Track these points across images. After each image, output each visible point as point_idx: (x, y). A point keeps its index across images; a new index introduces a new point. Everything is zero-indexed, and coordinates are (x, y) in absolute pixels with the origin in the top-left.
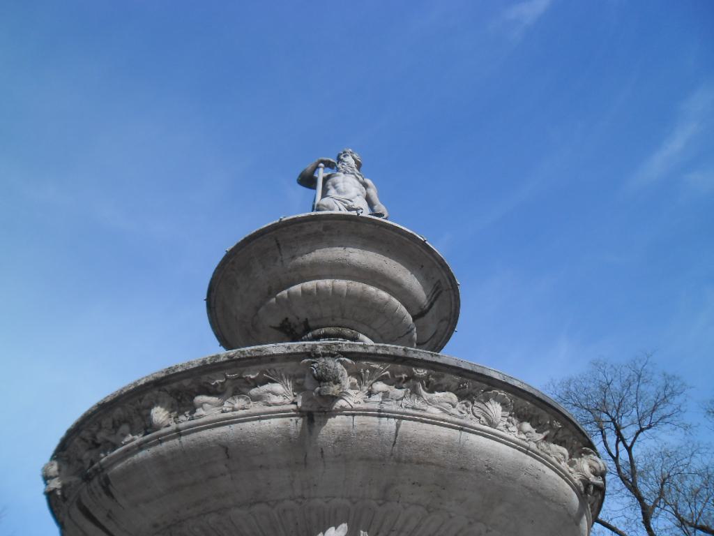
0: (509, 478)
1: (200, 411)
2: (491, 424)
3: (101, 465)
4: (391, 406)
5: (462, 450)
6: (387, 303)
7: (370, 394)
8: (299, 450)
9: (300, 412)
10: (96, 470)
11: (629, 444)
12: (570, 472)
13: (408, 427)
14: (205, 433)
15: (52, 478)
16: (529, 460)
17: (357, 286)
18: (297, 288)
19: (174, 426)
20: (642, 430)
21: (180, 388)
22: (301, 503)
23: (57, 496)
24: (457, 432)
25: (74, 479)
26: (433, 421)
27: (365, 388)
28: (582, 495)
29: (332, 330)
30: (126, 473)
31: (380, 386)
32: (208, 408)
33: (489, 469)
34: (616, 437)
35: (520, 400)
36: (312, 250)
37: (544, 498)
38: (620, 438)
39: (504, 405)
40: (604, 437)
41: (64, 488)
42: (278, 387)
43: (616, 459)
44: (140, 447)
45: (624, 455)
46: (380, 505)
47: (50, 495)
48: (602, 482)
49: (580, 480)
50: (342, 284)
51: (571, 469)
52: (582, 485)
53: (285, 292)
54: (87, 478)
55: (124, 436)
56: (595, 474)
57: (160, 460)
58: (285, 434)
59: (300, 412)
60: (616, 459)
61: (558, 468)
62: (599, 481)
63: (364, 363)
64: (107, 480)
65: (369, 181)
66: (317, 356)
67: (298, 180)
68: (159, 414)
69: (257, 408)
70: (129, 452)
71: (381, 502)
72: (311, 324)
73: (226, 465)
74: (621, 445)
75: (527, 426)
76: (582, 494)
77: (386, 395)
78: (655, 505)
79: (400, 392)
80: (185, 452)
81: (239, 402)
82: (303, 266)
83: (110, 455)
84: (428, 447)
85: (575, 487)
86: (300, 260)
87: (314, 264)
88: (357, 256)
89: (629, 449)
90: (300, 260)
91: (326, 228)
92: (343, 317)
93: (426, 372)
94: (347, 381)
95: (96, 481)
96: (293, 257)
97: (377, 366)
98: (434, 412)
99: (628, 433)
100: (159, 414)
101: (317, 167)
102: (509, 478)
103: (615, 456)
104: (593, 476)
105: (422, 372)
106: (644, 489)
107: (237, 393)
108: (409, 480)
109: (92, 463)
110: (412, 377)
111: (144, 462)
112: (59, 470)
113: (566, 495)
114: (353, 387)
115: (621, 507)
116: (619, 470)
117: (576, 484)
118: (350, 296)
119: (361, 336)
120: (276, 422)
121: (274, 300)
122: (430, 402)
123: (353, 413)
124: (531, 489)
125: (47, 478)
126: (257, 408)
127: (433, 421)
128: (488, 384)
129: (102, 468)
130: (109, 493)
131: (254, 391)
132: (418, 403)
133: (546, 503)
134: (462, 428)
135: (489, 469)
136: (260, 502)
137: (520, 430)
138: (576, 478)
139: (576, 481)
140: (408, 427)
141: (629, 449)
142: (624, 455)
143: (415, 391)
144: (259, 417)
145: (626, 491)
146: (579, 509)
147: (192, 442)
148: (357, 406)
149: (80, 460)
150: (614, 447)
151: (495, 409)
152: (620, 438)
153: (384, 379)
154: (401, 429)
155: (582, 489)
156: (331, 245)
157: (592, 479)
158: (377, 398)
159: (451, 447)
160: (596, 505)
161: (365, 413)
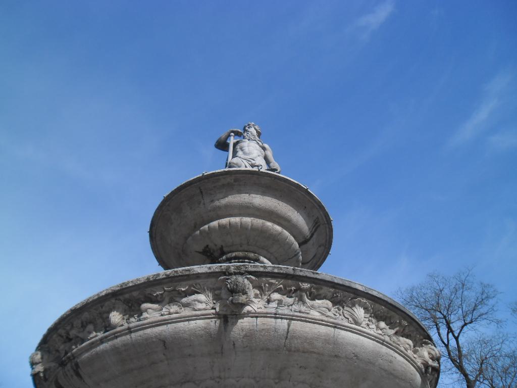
0: (371, 363)
1: (145, 315)
2: (357, 323)
3: (73, 355)
4: (284, 310)
6: (280, 234)
7: (269, 301)
8: (218, 342)
9: (218, 315)
10: (69, 358)
11: (456, 335)
12: (414, 357)
13: (297, 326)
14: (149, 331)
15: (37, 364)
16: (384, 349)
17: (258, 222)
18: (215, 224)
19: (126, 325)
20: (466, 324)
21: (130, 298)
22: (219, 382)
23: (40, 377)
25: (53, 364)
26: (314, 321)
27: (265, 298)
28: (423, 375)
29: (241, 254)
30: (91, 360)
31: (276, 296)
32: (151, 312)
34: (447, 329)
36: (224, 197)
37: (396, 377)
38: (450, 330)
39: (366, 309)
40: (438, 329)
41: (45, 371)
42: (202, 297)
43: (447, 346)
44: (102, 341)
45: (453, 343)
46: (276, 383)
47: (35, 376)
48: (438, 365)
49: (422, 363)
50: (247, 220)
51: (415, 356)
52: (423, 367)
53: (206, 226)
54: (62, 364)
55: (90, 333)
56: (433, 359)
57: (115, 350)
59: (218, 315)
60: (447, 346)
61: (405, 354)
62: (435, 364)
64: (77, 365)
65: (266, 146)
66: (231, 274)
67: (215, 145)
68: (115, 317)
69: (187, 312)
70: (93, 345)
71: (277, 381)
72: (225, 249)
73: (164, 354)
74: (450, 335)
75: (382, 324)
76: (423, 374)
77: (280, 302)
78: (476, 380)
79: (291, 300)
80: (134, 345)
81: (174, 308)
82: (219, 208)
83: (79, 347)
85: (418, 369)
86: (217, 203)
87: (227, 206)
88: (259, 200)
89: (457, 338)
90: (217, 203)
91: (236, 180)
92: (248, 244)
94: (252, 292)
95: (69, 366)
96: (212, 201)
98: (315, 314)
99: (456, 326)
100: (115, 317)
101: (229, 136)
103: (447, 344)
104: (431, 360)
105: (306, 286)
106: (468, 368)
107: (172, 301)
108: (297, 364)
109: (66, 353)
110: (298, 289)
111: (105, 352)
112: (42, 358)
113: (412, 374)
114: (256, 296)
115: (451, 381)
116: (449, 354)
117: (418, 367)
118: (254, 229)
119: (262, 258)
120: (201, 323)
121: (198, 232)
122: (313, 307)
123: (256, 315)
124: (386, 371)
125: (33, 364)
126: (187, 312)
127: (314, 321)
129: (74, 356)
130: (78, 375)
131: (184, 300)
133: (397, 380)
134: (336, 326)
136: (189, 381)
137: (378, 327)
138: (419, 362)
139: (419, 364)
141: (457, 338)
142: (453, 343)
143: (301, 299)
144: (188, 319)
145: (455, 369)
146: (421, 384)
149: (57, 351)
150: (446, 337)
151: (360, 312)
152: (450, 330)
155: (423, 370)
156: (240, 192)
157: (430, 362)
158: (274, 305)
159: (327, 340)
160: (434, 382)
161: (265, 315)
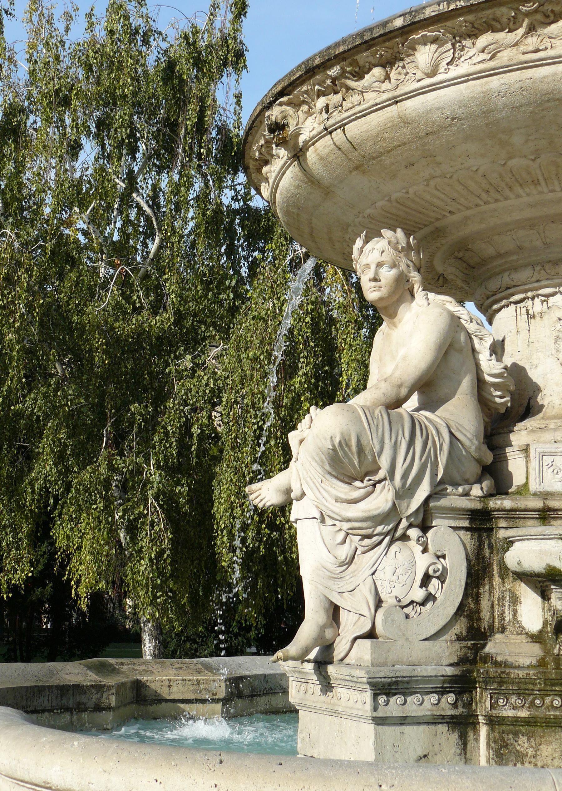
5: (405, 121)
13: (353, 129)
24: (394, 107)
33: (453, 119)
35: (449, 24)
58: (295, 177)
63: (296, 92)
84: (376, 138)
93: (339, 68)
97: (304, 88)
98: (371, 98)
102: (487, 113)
105: (334, 71)
128: (401, 35)
132: (356, 98)
135: (453, 119)
140: (353, 129)
147: (406, 130)
148: (315, 132)
153: (320, 94)
154: (337, 143)
